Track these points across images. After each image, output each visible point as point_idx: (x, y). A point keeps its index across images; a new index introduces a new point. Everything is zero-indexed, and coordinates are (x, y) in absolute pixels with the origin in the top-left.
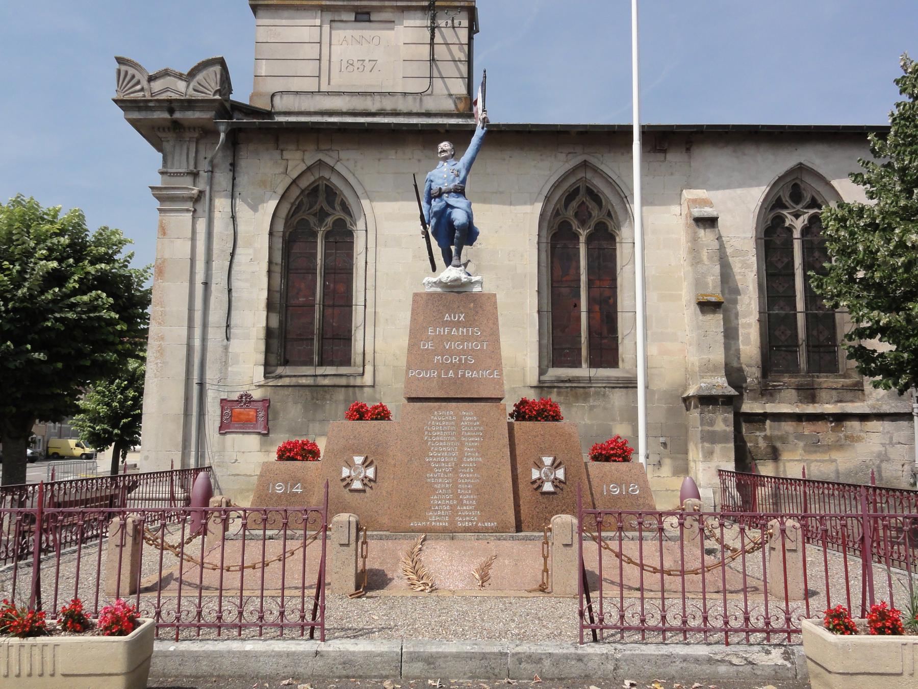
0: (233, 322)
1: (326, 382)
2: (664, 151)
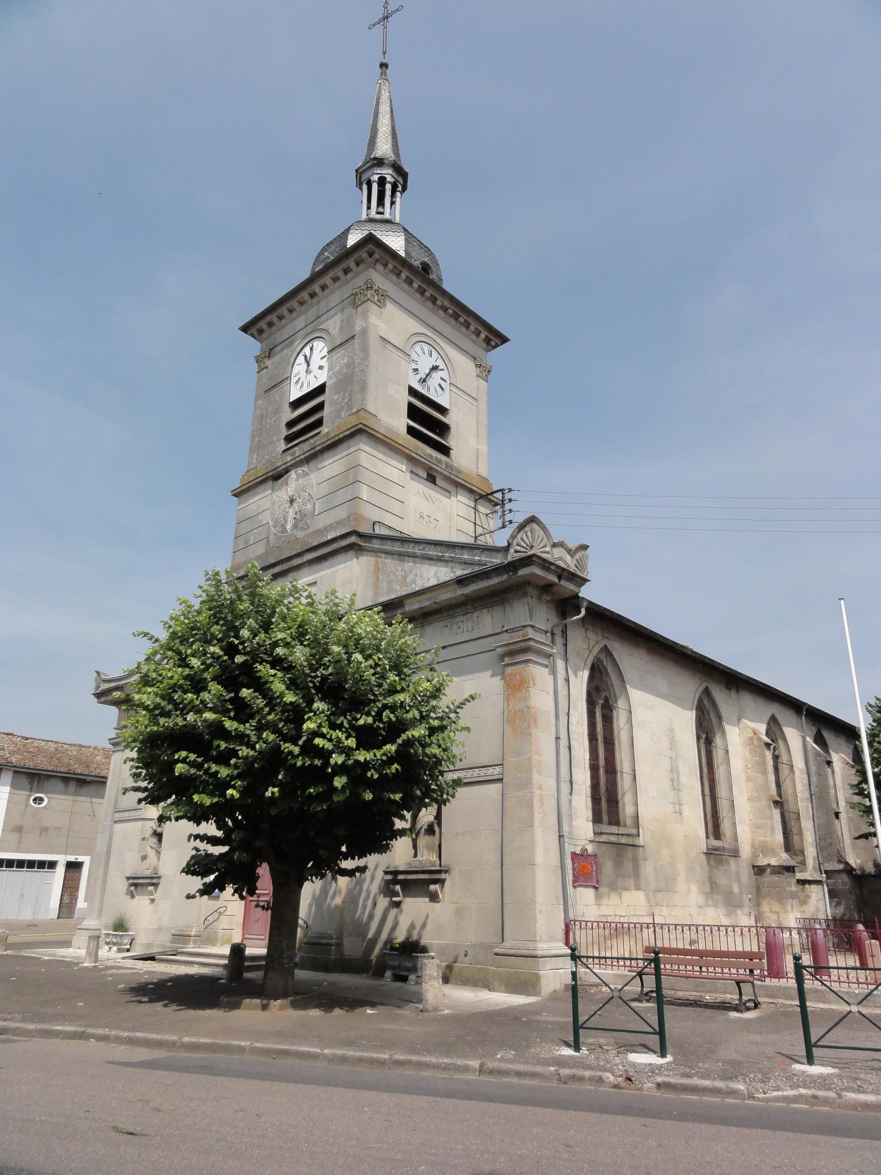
2: (729, 689)
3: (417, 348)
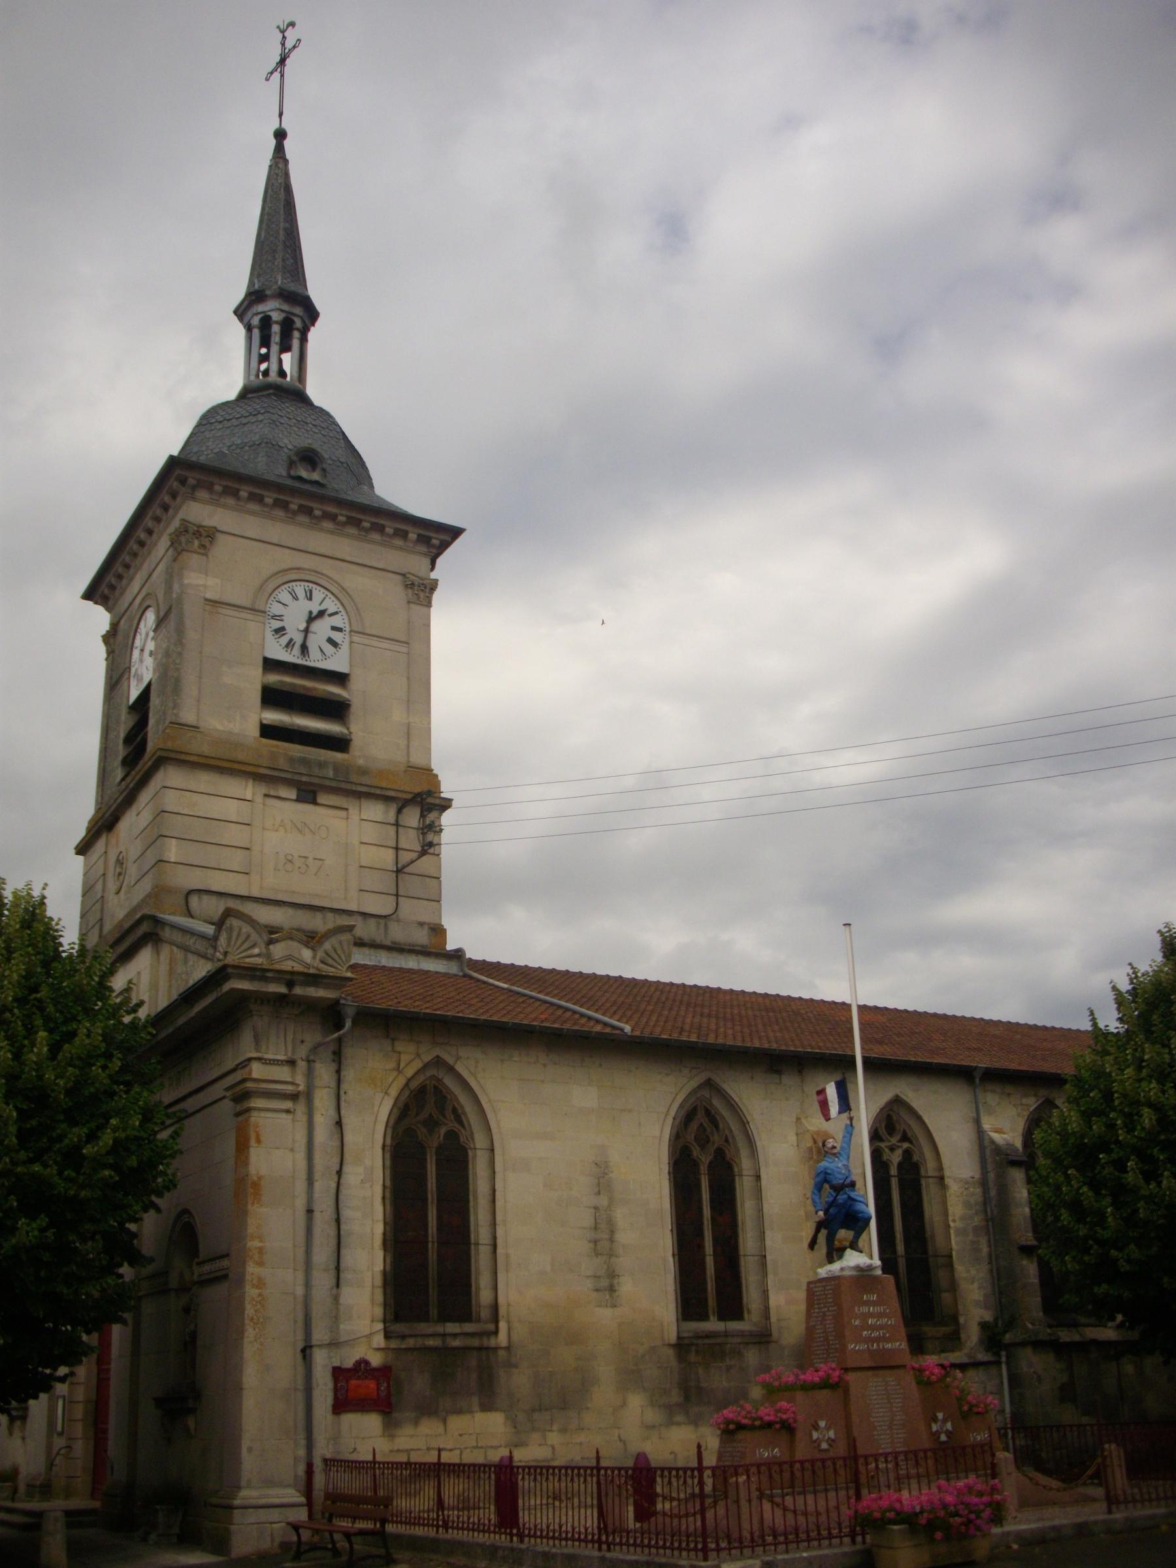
0: (342, 1265)
1: (456, 1343)
2: (779, 1072)
3: (284, 596)
